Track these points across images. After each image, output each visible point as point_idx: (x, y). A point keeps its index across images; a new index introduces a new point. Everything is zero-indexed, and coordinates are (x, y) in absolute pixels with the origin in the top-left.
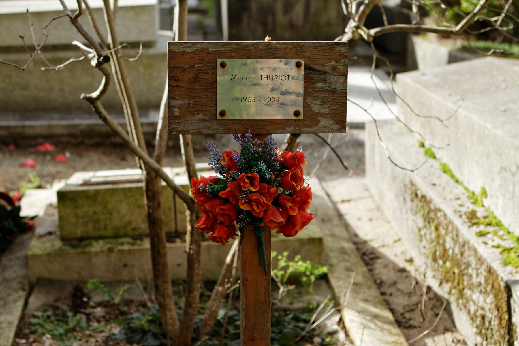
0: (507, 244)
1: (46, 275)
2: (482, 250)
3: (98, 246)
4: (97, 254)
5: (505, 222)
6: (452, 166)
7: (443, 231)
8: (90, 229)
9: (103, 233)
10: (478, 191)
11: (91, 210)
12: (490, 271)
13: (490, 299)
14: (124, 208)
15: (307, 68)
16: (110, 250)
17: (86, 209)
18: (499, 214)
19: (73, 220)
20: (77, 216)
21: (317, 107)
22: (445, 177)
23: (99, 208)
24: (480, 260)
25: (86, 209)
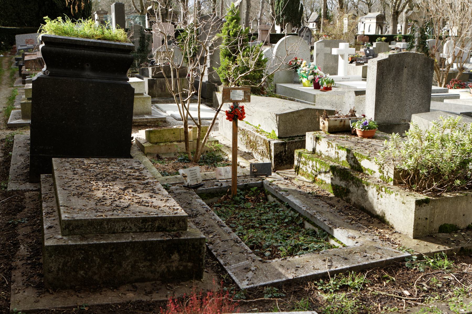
0: (267, 135)
1: (149, 152)
2: (261, 136)
3: (162, 144)
4: (162, 146)
5: (266, 131)
6: (249, 122)
7: (249, 136)
8: (159, 140)
9: (162, 141)
10: (257, 126)
11: (159, 135)
12: (264, 140)
13: (265, 147)
14: (167, 134)
15: (245, 92)
16: (166, 145)
17: (157, 135)
18: (264, 130)
19: (154, 138)
20: (155, 137)
21: (246, 98)
22: (247, 124)
23: (161, 135)
24: (261, 139)
25: (157, 135)
